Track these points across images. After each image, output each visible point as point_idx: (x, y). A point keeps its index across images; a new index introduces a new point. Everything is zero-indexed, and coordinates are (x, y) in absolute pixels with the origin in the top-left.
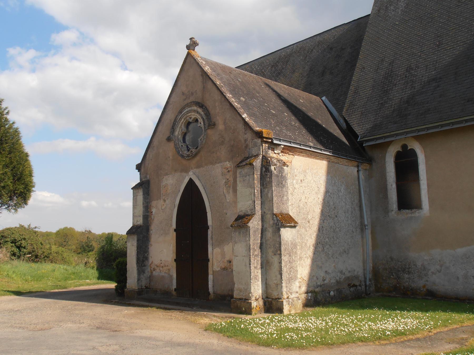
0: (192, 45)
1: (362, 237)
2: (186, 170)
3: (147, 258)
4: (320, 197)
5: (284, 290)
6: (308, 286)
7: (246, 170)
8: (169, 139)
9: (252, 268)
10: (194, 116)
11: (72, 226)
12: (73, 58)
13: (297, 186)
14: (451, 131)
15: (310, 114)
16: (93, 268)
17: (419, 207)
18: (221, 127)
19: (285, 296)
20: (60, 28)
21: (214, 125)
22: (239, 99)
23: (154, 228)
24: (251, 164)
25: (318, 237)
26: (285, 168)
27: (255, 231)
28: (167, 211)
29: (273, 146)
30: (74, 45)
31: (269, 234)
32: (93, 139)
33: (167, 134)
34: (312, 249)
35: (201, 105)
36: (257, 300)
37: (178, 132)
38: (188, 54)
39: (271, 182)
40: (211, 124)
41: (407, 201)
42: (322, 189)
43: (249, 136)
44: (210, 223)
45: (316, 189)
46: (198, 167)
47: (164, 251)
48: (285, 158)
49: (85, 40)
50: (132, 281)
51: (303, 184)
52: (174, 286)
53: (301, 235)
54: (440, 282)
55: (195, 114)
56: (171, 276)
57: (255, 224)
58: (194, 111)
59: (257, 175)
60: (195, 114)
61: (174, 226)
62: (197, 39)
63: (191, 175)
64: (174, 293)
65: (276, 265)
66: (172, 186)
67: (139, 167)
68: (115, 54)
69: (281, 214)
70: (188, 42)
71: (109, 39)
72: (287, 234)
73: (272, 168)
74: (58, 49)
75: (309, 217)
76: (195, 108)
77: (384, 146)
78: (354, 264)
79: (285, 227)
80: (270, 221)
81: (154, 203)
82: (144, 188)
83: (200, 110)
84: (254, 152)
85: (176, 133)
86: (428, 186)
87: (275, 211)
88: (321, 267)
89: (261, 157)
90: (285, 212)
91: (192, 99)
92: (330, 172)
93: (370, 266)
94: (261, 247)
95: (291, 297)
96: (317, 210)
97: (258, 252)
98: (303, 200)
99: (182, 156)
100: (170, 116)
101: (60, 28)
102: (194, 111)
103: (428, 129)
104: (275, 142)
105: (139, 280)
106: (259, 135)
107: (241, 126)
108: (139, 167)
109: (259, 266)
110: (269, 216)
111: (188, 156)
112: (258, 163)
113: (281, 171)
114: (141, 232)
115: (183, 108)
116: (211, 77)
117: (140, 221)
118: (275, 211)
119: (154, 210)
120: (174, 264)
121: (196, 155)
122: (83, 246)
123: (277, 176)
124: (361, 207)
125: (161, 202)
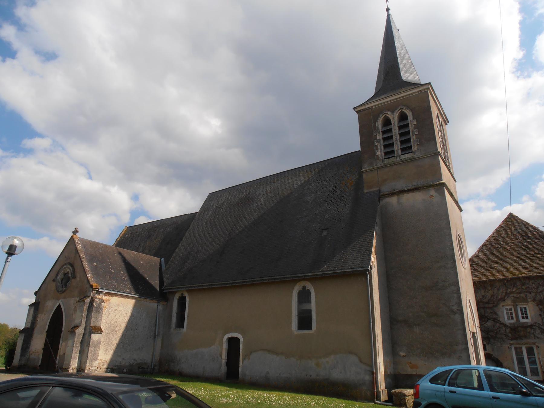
0: (75, 232)
1: (154, 342)
2: (58, 299)
3: (28, 347)
4: (127, 319)
5: (88, 365)
6: (109, 365)
7: (82, 303)
8: (54, 280)
9: (74, 352)
10: (68, 270)
11: (6, 323)
12: (41, 163)
13: (111, 313)
14: (205, 289)
15: (142, 271)
16: (2, 357)
17: (183, 327)
18: (78, 279)
19: (88, 368)
20: (33, 134)
21: (76, 277)
22: (92, 265)
23: (36, 330)
24: (84, 301)
25: (121, 339)
26: (103, 304)
27: (79, 335)
28: (44, 320)
29: (99, 293)
30: (45, 150)
31: (86, 337)
32: (46, 239)
33: (54, 277)
34: (115, 346)
35: (72, 265)
36: (73, 369)
37: (59, 278)
38: (72, 237)
39: (92, 311)
40: (74, 277)
41: (180, 324)
42: (129, 315)
43: (88, 286)
44: (63, 329)
45: (125, 314)
46: (65, 298)
47: (38, 343)
48: (105, 298)
49: (56, 146)
50: (16, 361)
51: (116, 312)
52: (40, 364)
53: (109, 338)
54: (185, 368)
55: (68, 269)
56: (39, 358)
57: (80, 331)
58: (69, 268)
59: (86, 307)
60: (68, 269)
61: (46, 330)
62: (78, 230)
63: (60, 302)
64: (38, 368)
65: (87, 352)
66: (51, 306)
67: (36, 293)
68: (82, 164)
69: (95, 327)
70: (74, 230)
71: (80, 151)
72: (95, 337)
73: (94, 304)
74: (29, 152)
75: (117, 329)
76: (69, 266)
77: (174, 293)
78: (145, 355)
79: (94, 333)
80: (88, 330)
81: (39, 315)
82: (35, 307)
83: (71, 268)
84: (88, 295)
85: (58, 278)
86: (316, 314)
87: (92, 325)
88: (120, 356)
89: (90, 298)
90: (98, 325)
91: (68, 262)
92: (135, 306)
93: (157, 357)
94: (82, 343)
95: (91, 368)
96: (124, 325)
97: (79, 345)
98: (114, 320)
99: (58, 291)
100: (57, 268)
101: (33, 134)
102: (69, 268)
103: (198, 286)
104: (100, 290)
105: (20, 360)
106: (91, 286)
107: (86, 281)
108: (36, 293)
109: (78, 352)
110: (88, 327)
111: (61, 291)
112: (88, 300)
113: (100, 304)
114: (28, 333)
115: (64, 265)
116: (79, 252)
117: (29, 325)
118: (92, 325)
119: (38, 320)
120: (42, 351)
121: (65, 291)
122: (9, 343)
123: (97, 308)
124: (156, 325)
125: (43, 315)
